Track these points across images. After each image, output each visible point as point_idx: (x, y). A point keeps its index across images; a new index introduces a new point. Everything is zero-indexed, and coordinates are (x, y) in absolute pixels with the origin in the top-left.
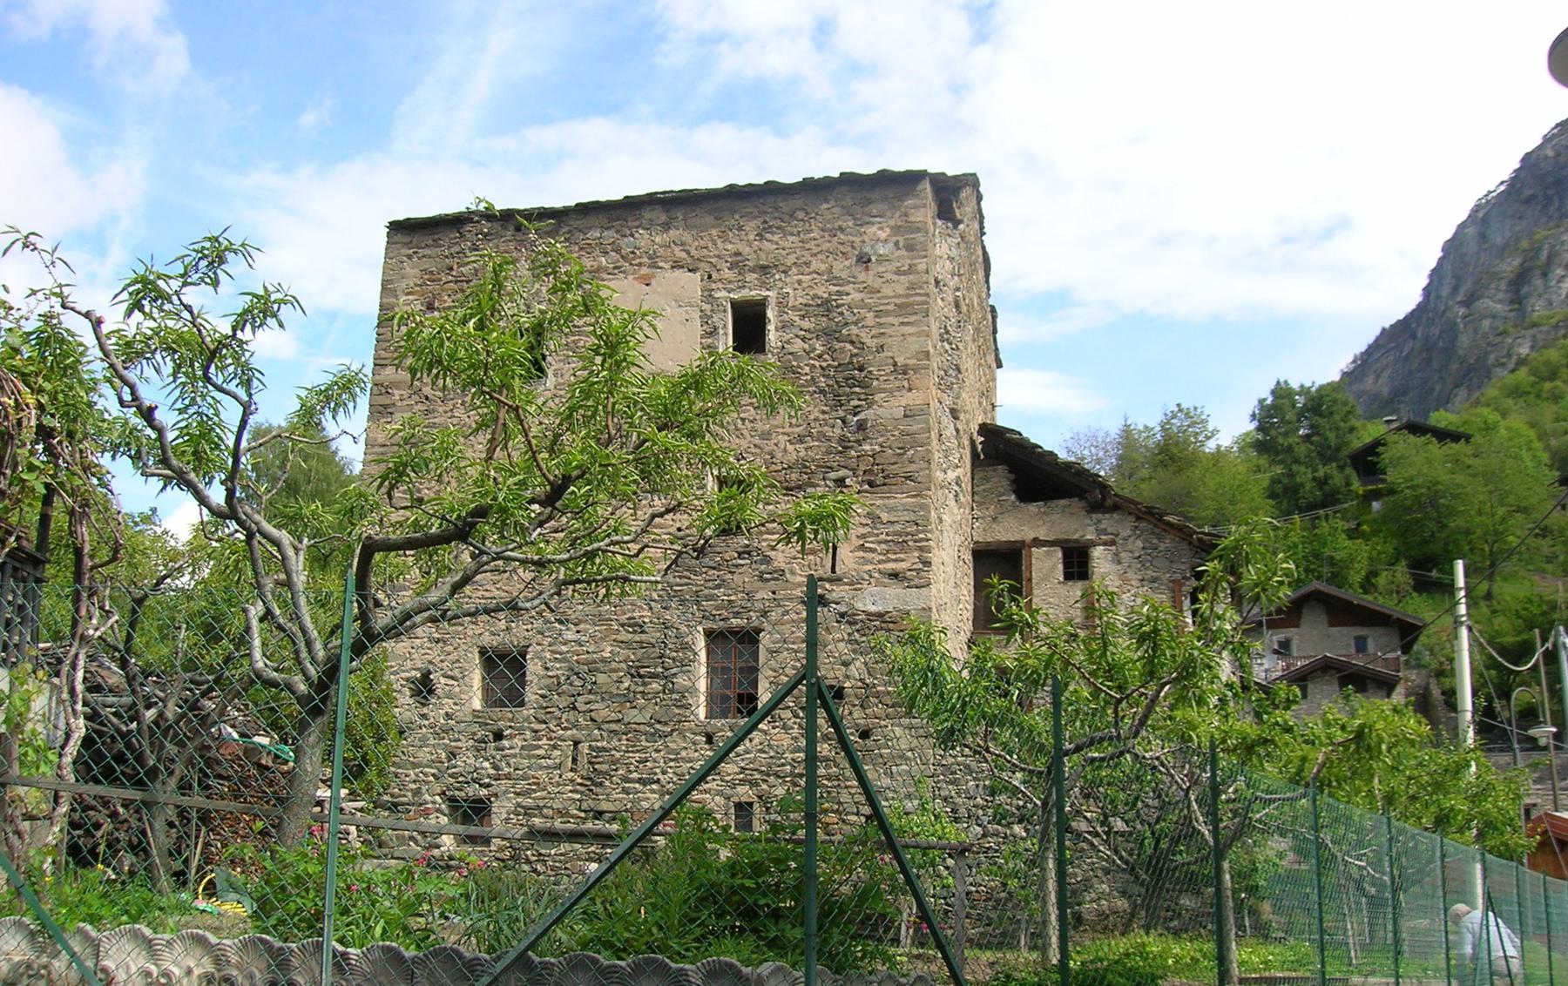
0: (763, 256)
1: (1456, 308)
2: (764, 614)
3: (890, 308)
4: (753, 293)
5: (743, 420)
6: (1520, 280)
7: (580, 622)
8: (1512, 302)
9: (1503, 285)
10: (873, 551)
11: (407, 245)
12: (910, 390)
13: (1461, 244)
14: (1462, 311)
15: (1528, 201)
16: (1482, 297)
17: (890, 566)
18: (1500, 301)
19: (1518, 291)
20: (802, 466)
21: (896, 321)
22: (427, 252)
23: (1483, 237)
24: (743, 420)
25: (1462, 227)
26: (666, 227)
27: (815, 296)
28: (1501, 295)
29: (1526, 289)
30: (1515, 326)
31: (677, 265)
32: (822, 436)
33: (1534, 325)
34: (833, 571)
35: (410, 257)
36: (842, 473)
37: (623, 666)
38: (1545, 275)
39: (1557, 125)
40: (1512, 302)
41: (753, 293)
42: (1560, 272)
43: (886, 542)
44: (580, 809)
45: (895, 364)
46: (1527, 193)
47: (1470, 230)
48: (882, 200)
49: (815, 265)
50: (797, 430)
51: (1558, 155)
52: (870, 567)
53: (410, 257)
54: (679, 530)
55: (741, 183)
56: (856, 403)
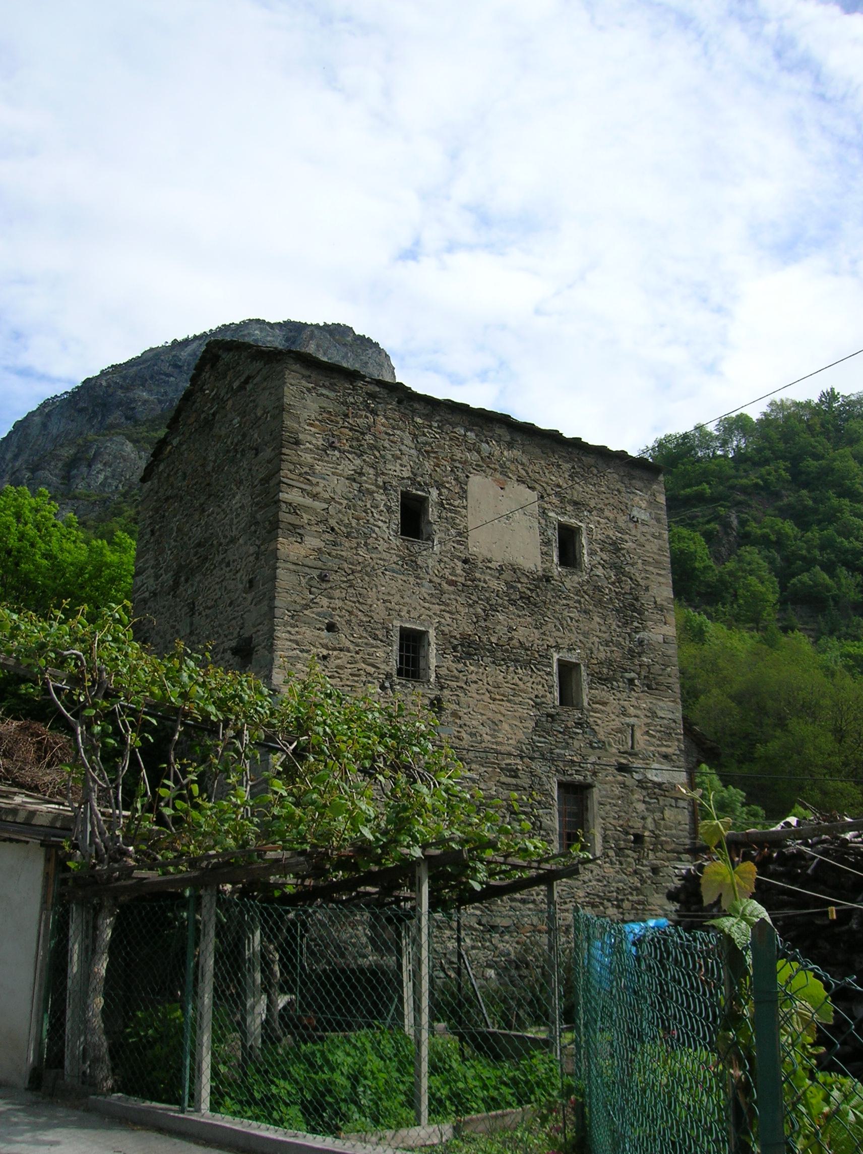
0: (575, 494)
1: (24, 472)
2: (595, 774)
3: (651, 560)
4: (572, 521)
5: (571, 619)
6: (72, 463)
7: (472, 761)
8: (63, 478)
9: (60, 465)
10: (654, 737)
11: (308, 378)
12: (665, 624)
13: (28, 427)
14: (28, 474)
15: (80, 411)
16: (44, 469)
17: (664, 749)
18: (56, 476)
19: (69, 472)
20: (609, 663)
21: (655, 571)
22: (324, 392)
23: (44, 426)
24: (571, 619)
25: (31, 415)
26: (510, 445)
27: (608, 537)
28: (57, 471)
29: (75, 472)
30: (62, 495)
31: (521, 481)
32: (618, 644)
33: (75, 498)
34: (632, 748)
35: (309, 390)
36: (633, 675)
37: (505, 803)
38: (90, 466)
39: (113, 366)
40: (63, 478)
41: (572, 521)
42: (100, 466)
43: (660, 731)
44: (480, 924)
45: (655, 603)
46: (82, 405)
47: (37, 419)
48: (641, 479)
49: (607, 513)
50: (604, 635)
51: (109, 386)
52: (652, 748)
53: (309, 390)
54: (537, 696)
55: (440, 398)
56: (635, 624)
